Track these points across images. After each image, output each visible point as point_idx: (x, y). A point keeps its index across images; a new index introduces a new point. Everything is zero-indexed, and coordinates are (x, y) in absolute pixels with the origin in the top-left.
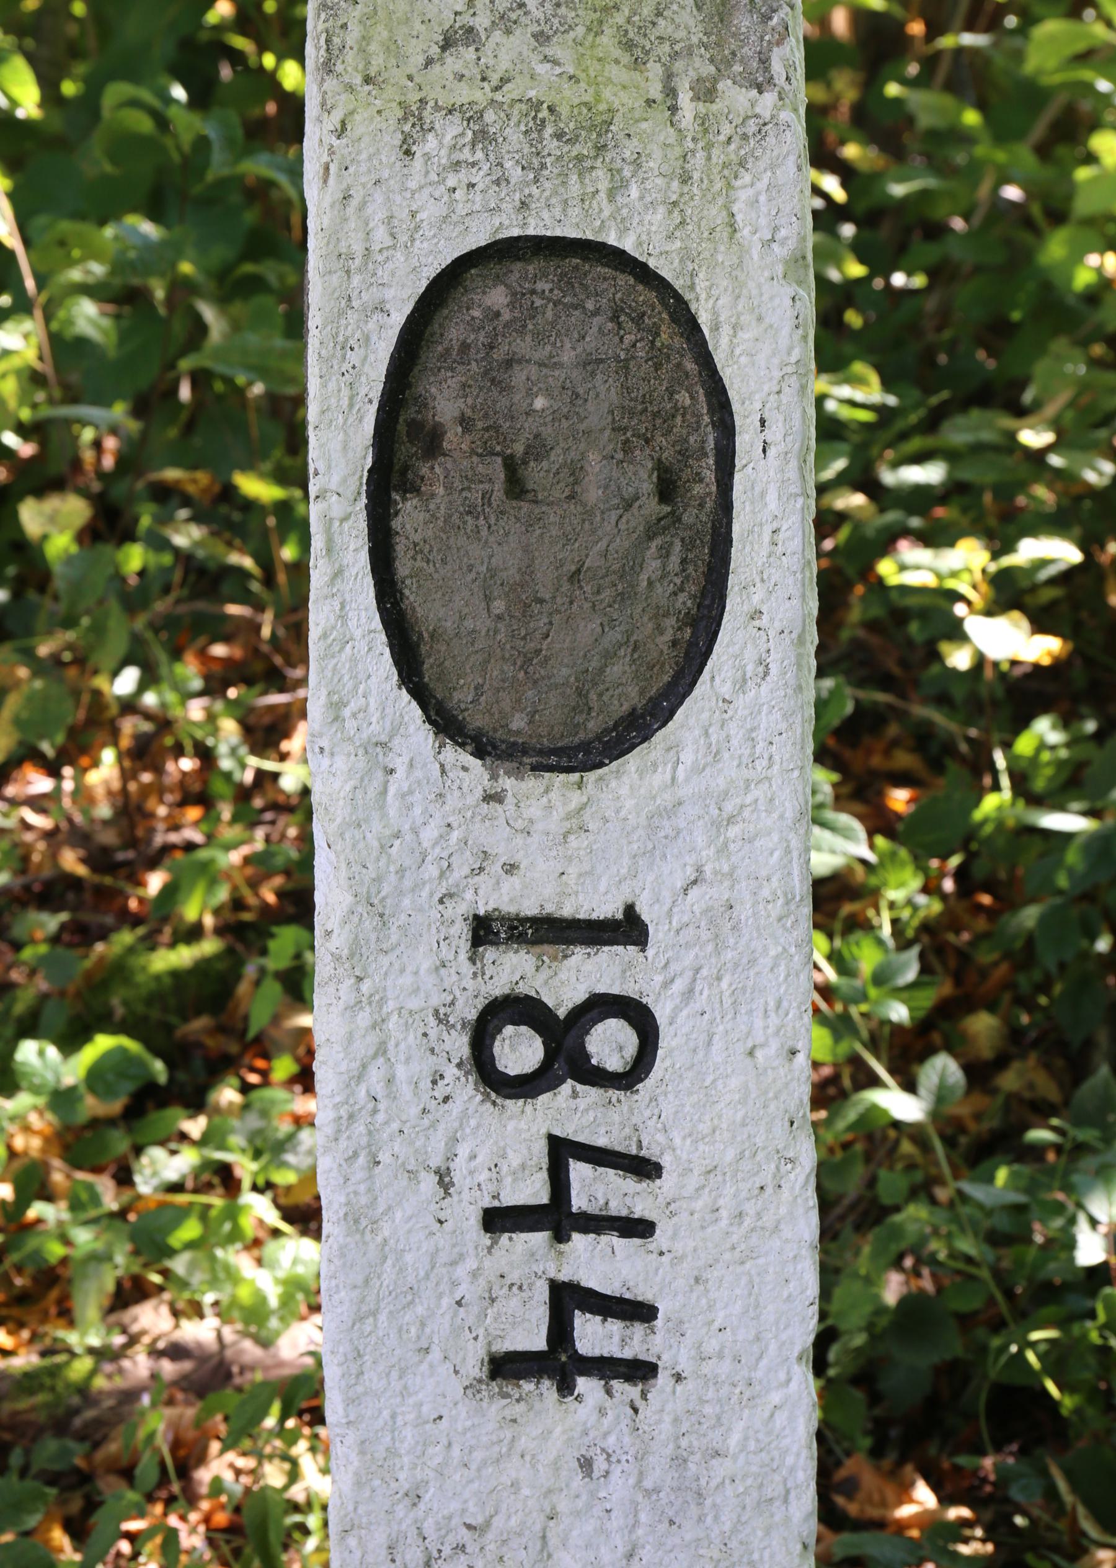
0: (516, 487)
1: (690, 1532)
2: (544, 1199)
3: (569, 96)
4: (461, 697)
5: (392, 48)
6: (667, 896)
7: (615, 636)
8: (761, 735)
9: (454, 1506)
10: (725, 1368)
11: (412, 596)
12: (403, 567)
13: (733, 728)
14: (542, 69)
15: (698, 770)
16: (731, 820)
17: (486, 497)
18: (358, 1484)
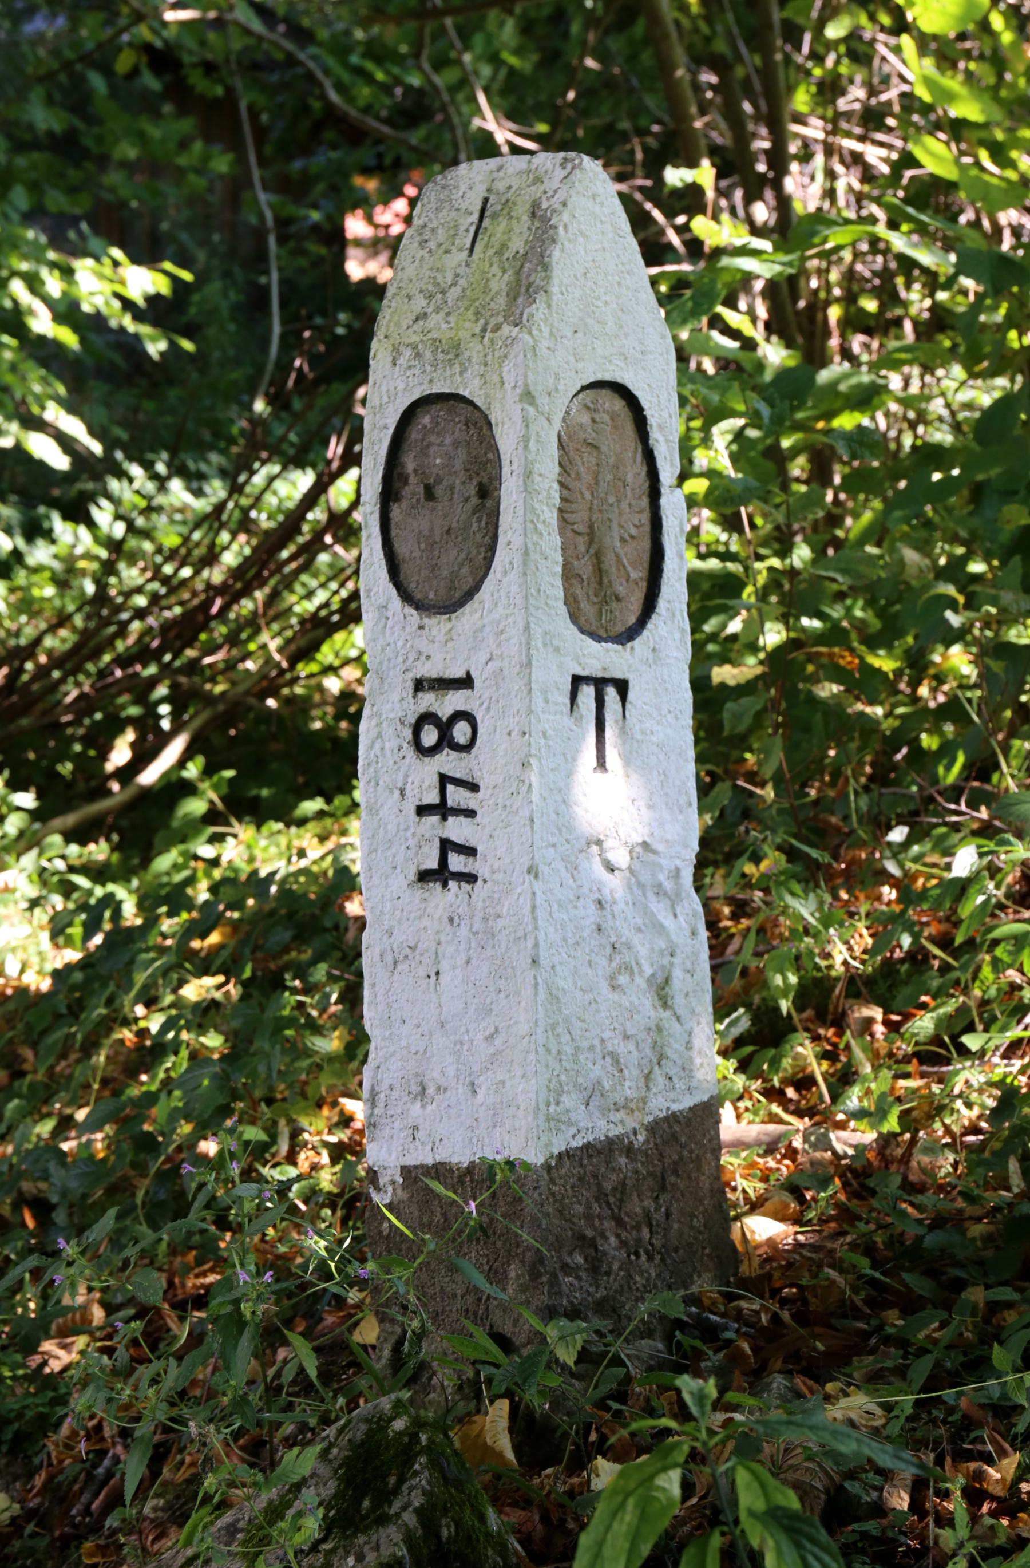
1: (489, 952)
2: (437, 801)
7: (462, 556)
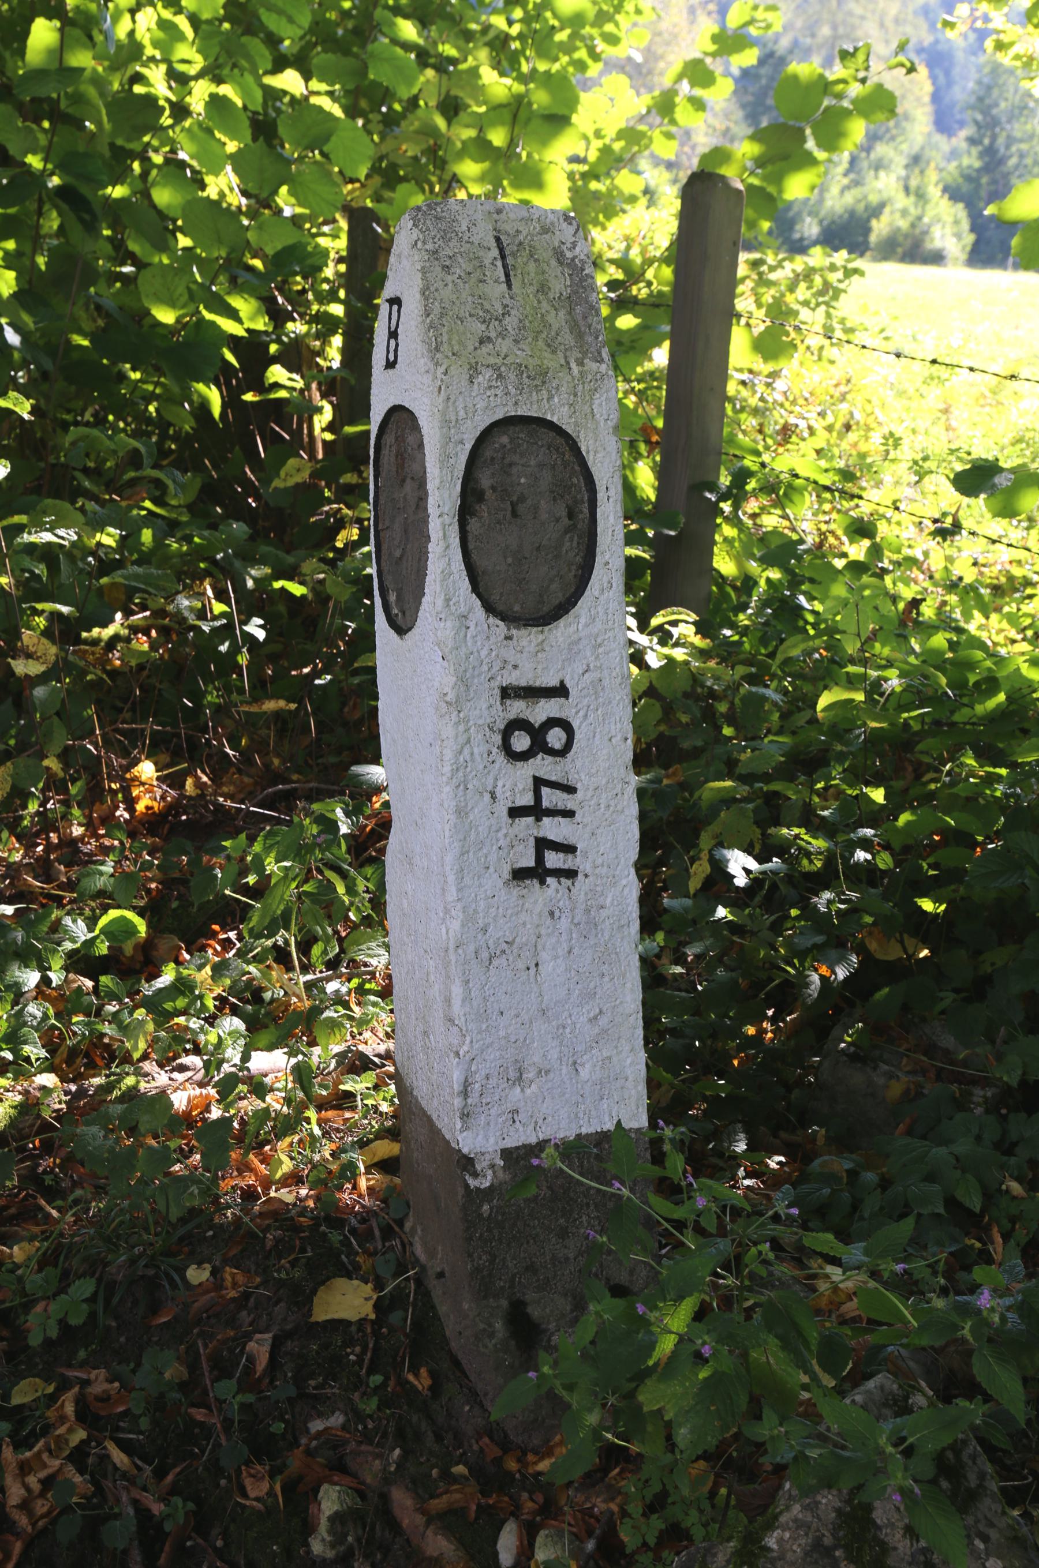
0: (515, 514)
3: (532, 363)
4: (495, 597)
5: (461, 343)
6: (576, 677)
8: (610, 611)
9: (501, 934)
10: (604, 870)
11: (474, 556)
12: (471, 546)
13: (599, 609)
14: (519, 353)
15: (587, 625)
16: (600, 645)
17: (504, 516)
18: (463, 926)
